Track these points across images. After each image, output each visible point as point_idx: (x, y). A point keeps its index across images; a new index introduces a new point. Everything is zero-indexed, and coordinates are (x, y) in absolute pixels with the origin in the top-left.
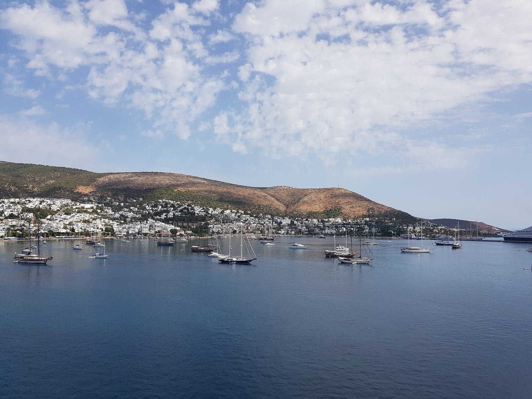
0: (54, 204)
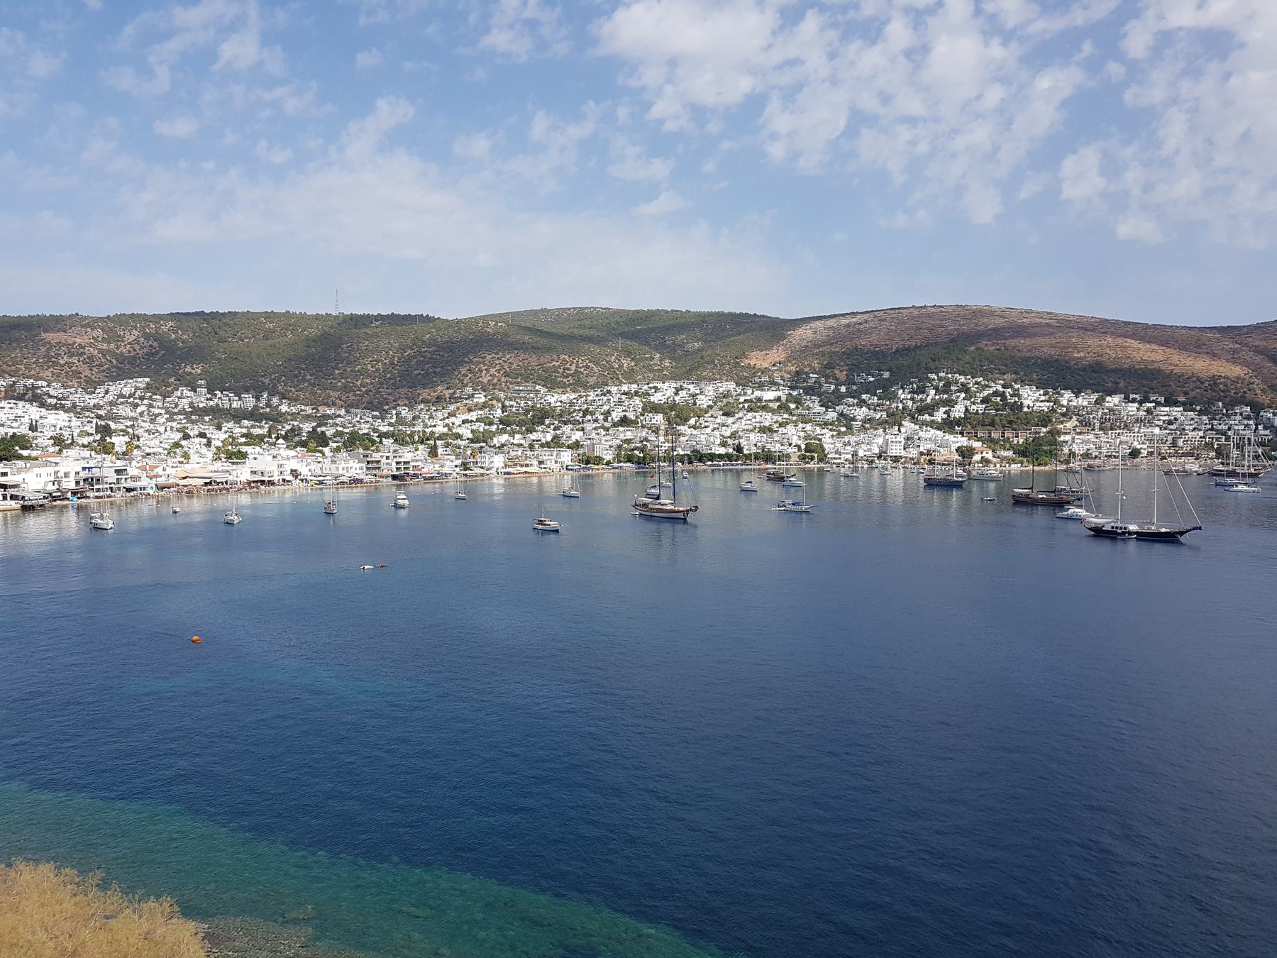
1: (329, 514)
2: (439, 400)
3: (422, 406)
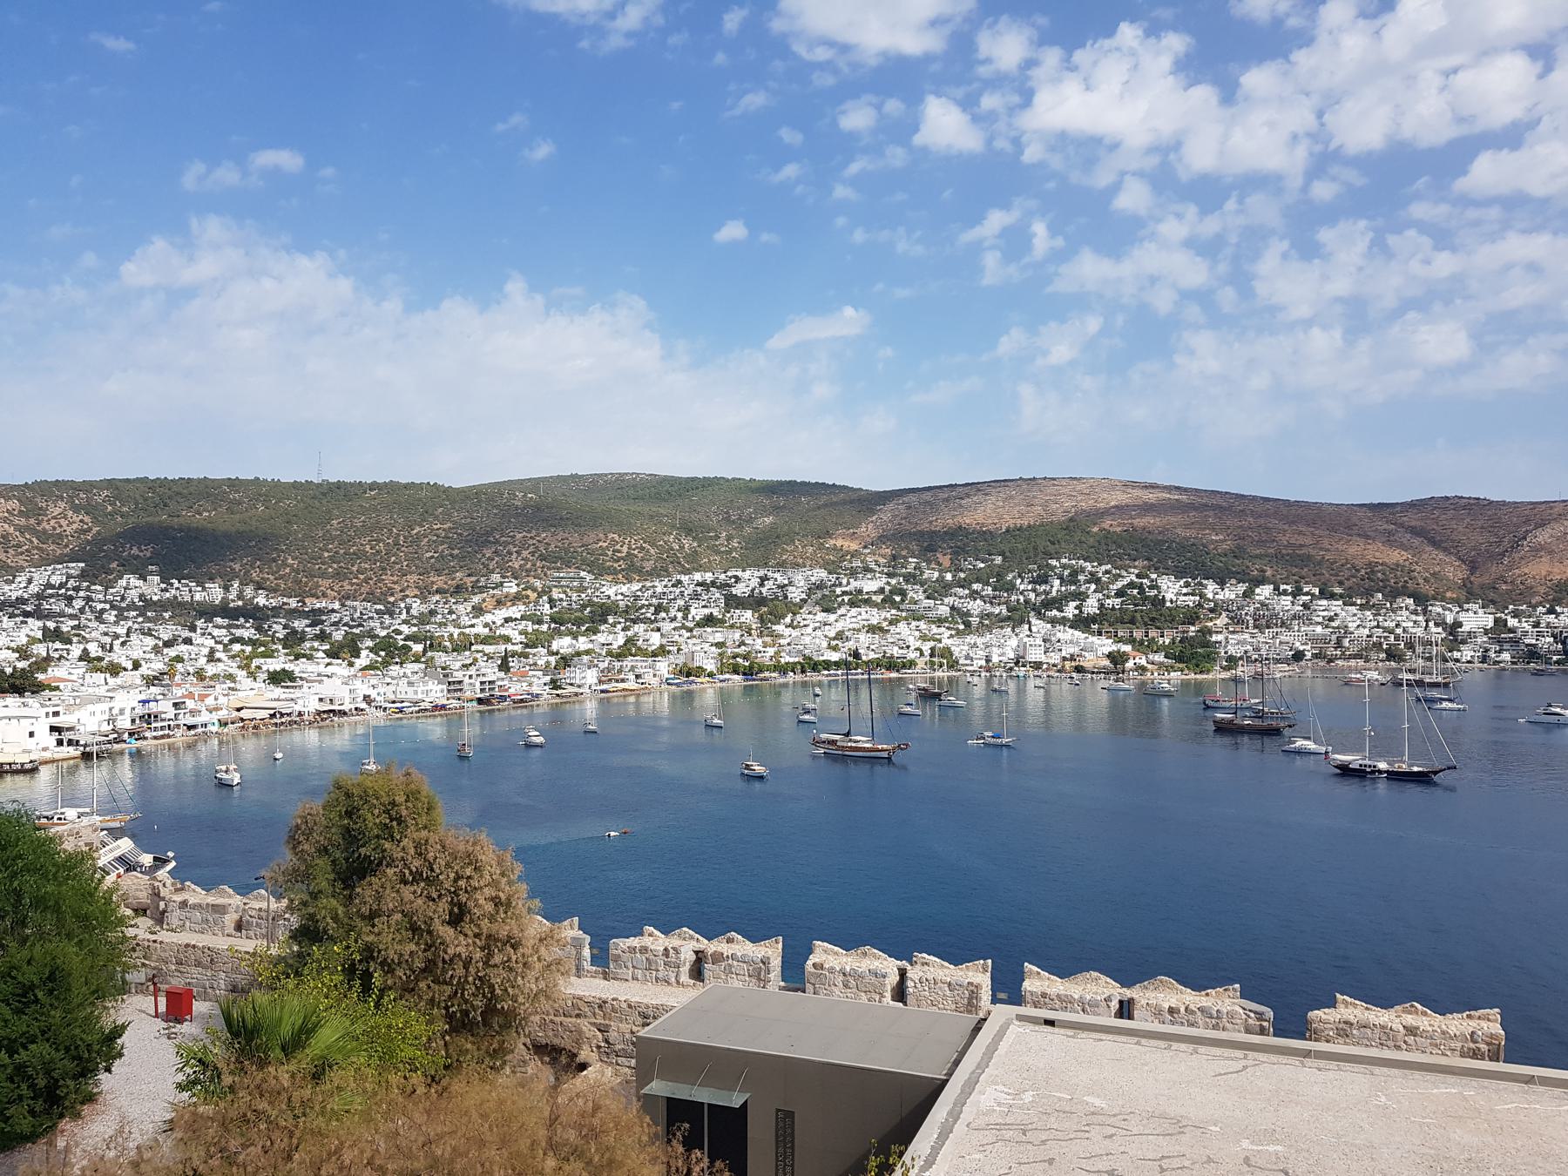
1: (462, 758)
2: (458, 590)
3: (437, 597)
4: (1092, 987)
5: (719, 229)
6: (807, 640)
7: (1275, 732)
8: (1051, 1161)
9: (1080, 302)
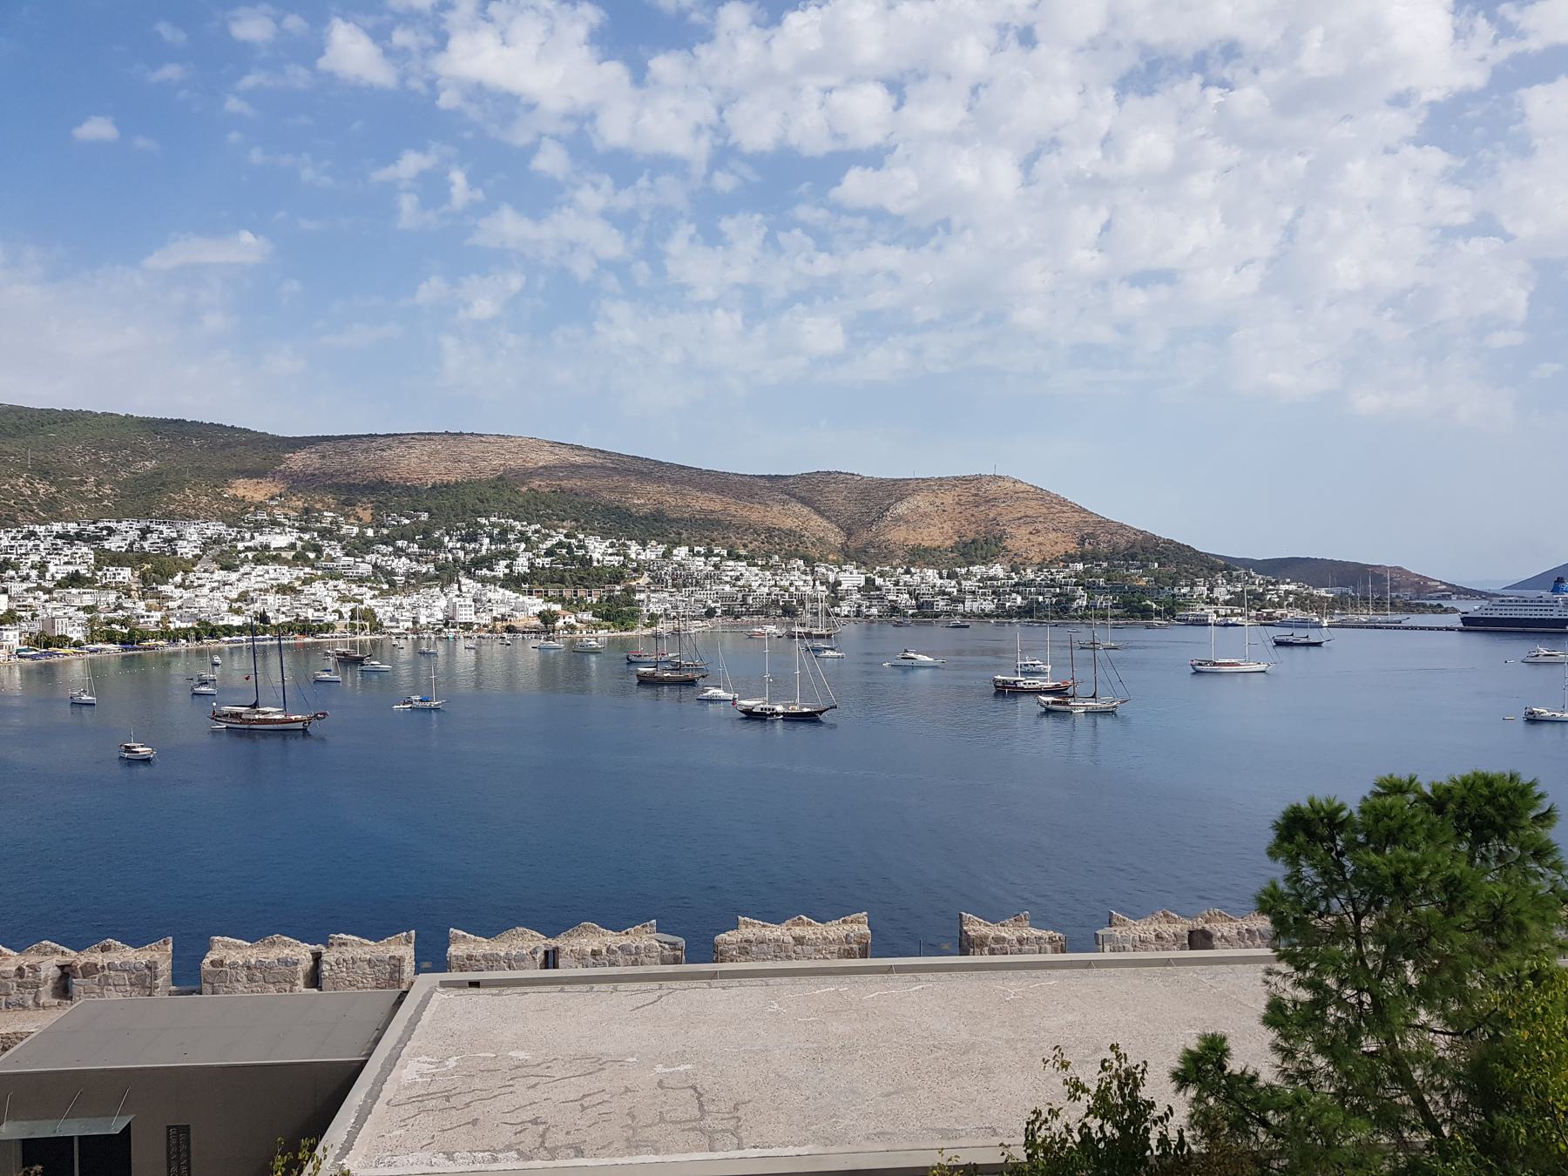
0: (180, 537)
4: (518, 942)
5: (79, 123)
6: (203, 602)
7: (691, 683)
8: (475, 1122)
9: (498, 259)
